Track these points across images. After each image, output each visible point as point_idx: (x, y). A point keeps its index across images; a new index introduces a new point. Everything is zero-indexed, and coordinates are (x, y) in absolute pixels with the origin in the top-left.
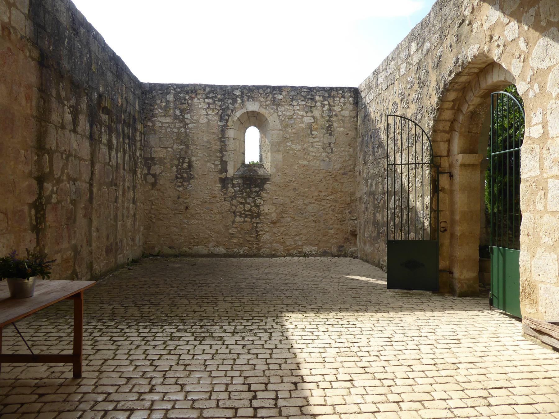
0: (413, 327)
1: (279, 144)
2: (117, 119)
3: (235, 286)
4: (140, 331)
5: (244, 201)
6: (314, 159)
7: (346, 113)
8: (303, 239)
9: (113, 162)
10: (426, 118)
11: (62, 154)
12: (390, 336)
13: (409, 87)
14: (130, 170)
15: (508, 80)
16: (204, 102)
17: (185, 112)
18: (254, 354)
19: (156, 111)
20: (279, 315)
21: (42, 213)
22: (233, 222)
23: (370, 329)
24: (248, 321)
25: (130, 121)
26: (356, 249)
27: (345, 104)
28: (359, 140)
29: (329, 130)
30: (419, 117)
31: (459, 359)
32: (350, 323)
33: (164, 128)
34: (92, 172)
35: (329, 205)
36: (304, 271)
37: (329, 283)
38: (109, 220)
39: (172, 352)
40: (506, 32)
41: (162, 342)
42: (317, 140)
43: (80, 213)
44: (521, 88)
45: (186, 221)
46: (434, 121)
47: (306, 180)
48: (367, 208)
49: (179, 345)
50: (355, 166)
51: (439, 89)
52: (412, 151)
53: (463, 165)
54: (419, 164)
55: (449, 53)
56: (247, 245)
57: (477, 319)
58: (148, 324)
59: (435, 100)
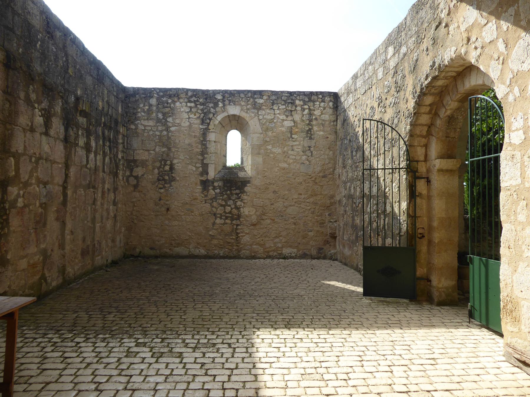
0: (386, 343)
1: (259, 147)
2: (96, 122)
3: (209, 291)
4: (97, 345)
5: (224, 203)
6: (294, 162)
7: (326, 117)
8: (283, 241)
9: (91, 165)
10: (403, 123)
11: (31, 157)
12: (361, 354)
13: (386, 91)
14: (110, 172)
15: (486, 83)
16: (186, 106)
17: (167, 115)
18: (211, 375)
19: (139, 115)
20: (247, 326)
21: (5, 217)
22: (214, 224)
23: (341, 345)
24: (213, 333)
25: (111, 124)
26: (335, 251)
27: (324, 108)
28: (339, 143)
29: (310, 134)
30: (396, 121)
31: (435, 385)
32: (321, 336)
33: (146, 131)
34: (67, 175)
35: (309, 208)
36: (281, 275)
37: (304, 289)
38: (86, 222)
39: (124, 373)
40: (484, 34)
41: (116, 359)
42: (297, 143)
43: (51, 216)
44: (500, 91)
45: (167, 222)
46: (411, 125)
47: (286, 183)
48: (346, 211)
49: (134, 363)
50: (334, 169)
51: (416, 93)
52: (389, 155)
53: (440, 171)
54: (396, 169)
55: (426, 56)
56: (227, 247)
57: (456, 333)
58: (107, 336)
59: (411, 104)
